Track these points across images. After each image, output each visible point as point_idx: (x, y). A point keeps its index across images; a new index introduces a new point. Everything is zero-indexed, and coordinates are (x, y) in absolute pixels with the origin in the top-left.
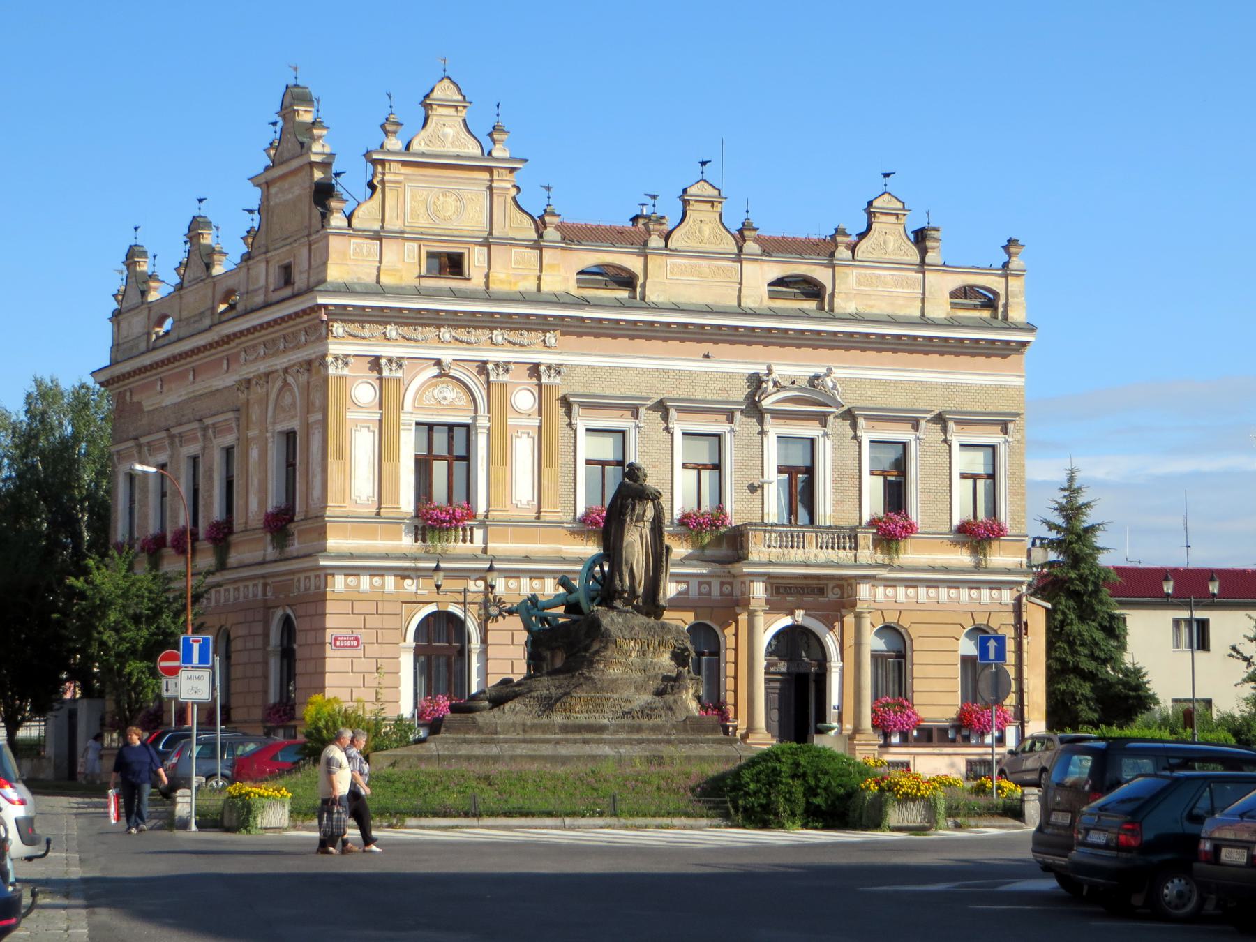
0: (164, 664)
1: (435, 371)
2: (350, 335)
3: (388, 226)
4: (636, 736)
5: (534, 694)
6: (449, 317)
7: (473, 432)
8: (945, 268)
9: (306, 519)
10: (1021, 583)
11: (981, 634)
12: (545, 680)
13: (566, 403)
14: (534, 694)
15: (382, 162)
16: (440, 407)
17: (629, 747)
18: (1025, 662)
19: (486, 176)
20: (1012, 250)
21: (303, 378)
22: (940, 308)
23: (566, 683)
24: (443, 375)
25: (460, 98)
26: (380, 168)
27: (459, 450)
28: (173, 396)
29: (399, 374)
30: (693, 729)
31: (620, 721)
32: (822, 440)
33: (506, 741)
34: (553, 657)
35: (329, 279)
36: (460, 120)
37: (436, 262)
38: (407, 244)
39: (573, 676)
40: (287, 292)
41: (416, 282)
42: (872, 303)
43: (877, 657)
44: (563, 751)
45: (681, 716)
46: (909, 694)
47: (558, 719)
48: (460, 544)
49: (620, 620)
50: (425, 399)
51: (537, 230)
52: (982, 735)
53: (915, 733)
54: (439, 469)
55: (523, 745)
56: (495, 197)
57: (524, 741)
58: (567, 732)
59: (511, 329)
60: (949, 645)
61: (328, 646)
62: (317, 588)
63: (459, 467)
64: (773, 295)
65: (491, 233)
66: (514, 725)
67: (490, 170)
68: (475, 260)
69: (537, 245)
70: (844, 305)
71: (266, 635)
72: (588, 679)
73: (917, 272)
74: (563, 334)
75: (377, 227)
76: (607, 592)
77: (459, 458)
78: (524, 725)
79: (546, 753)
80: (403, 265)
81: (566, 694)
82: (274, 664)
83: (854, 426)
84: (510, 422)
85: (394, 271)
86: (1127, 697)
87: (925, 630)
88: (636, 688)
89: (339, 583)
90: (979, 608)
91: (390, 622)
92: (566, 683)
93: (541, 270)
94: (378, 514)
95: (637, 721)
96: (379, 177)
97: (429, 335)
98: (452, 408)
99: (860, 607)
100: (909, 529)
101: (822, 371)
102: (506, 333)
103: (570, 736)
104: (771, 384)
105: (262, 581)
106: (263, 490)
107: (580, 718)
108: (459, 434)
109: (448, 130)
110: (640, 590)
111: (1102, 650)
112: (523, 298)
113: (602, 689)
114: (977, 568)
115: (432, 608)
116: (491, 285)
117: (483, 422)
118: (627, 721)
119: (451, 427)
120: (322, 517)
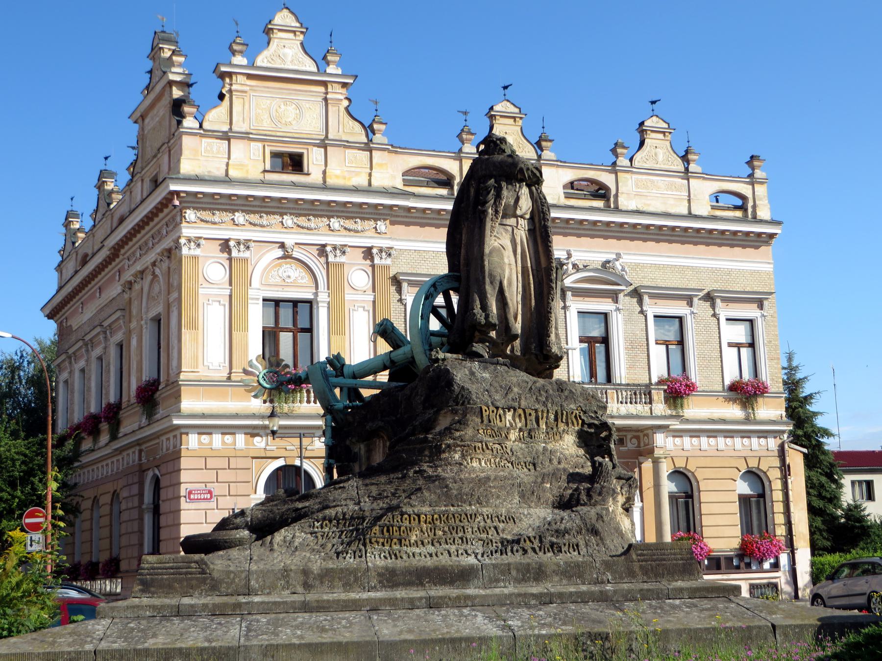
0: (28, 521)
1: (280, 253)
2: (202, 220)
3: (235, 128)
4: (535, 590)
5: (331, 512)
6: (291, 205)
7: (315, 307)
8: (705, 176)
9: (167, 385)
10: (783, 432)
11: (754, 475)
12: (353, 484)
13: (397, 282)
14: (331, 512)
15: (230, 75)
16: (285, 283)
17: (525, 613)
18: (791, 499)
19: (322, 89)
20: (756, 163)
21: (165, 265)
22: (702, 207)
23: (391, 489)
24: (287, 256)
25: (298, 25)
26: (227, 80)
27: (303, 323)
28: (89, 313)
29: (247, 254)
30: (645, 571)
31: (497, 559)
32: (614, 314)
33: (266, 609)
34: (369, 451)
35: (182, 171)
36: (298, 43)
37: (279, 161)
38: (253, 144)
39: (404, 477)
41: (261, 176)
42: (648, 202)
43: (673, 497)
45: (616, 546)
46: (698, 529)
47: (376, 559)
48: (305, 404)
49: (486, 375)
50: (271, 277)
51: (367, 136)
52: (761, 562)
53: (706, 562)
54: (286, 339)
55: (302, 617)
56: (330, 107)
57: (306, 607)
59: (348, 218)
60: (729, 485)
61: (183, 500)
62: (175, 447)
63: (303, 337)
64: (568, 196)
65: (327, 136)
66: (286, 572)
67: (324, 84)
68: (314, 159)
69: (368, 147)
70: (624, 203)
71: (141, 495)
72: (431, 479)
73: (683, 179)
74: (393, 223)
75: (226, 128)
76: (462, 333)
77: (304, 330)
78: (306, 572)
79: (346, 636)
80: (250, 162)
81: (391, 509)
82: (148, 519)
83: (640, 302)
84: (347, 297)
85: (241, 166)
86: (854, 527)
87: (708, 473)
88: (522, 496)
89: (192, 441)
90: (751, 454)
91: (242, 476)
92: (391, 489)
93: (371, 168)
94: (229, 378)
95: (532, 558)
96: (227, 87)
97: (273, 222)
98: (295, 285)
99: (657, 453)
100: (691, 388)
101: (612, 257)
102: (342, 222)
103: (400, 593)
104: (570, 266)
105: (138, 448)
106: (140, 370)
107: (420, 554)
108: (303, 309)
109: (286, 50)
110: (517, 327)
111: (827, 491)
112: (356, 190)
113: (461, 499)
114: (747, 420)
115: (280, 463)
116: (328, 180)
117: (323, 297)
118: (514, 558)
119: (295, 303)
120: (177, 381)
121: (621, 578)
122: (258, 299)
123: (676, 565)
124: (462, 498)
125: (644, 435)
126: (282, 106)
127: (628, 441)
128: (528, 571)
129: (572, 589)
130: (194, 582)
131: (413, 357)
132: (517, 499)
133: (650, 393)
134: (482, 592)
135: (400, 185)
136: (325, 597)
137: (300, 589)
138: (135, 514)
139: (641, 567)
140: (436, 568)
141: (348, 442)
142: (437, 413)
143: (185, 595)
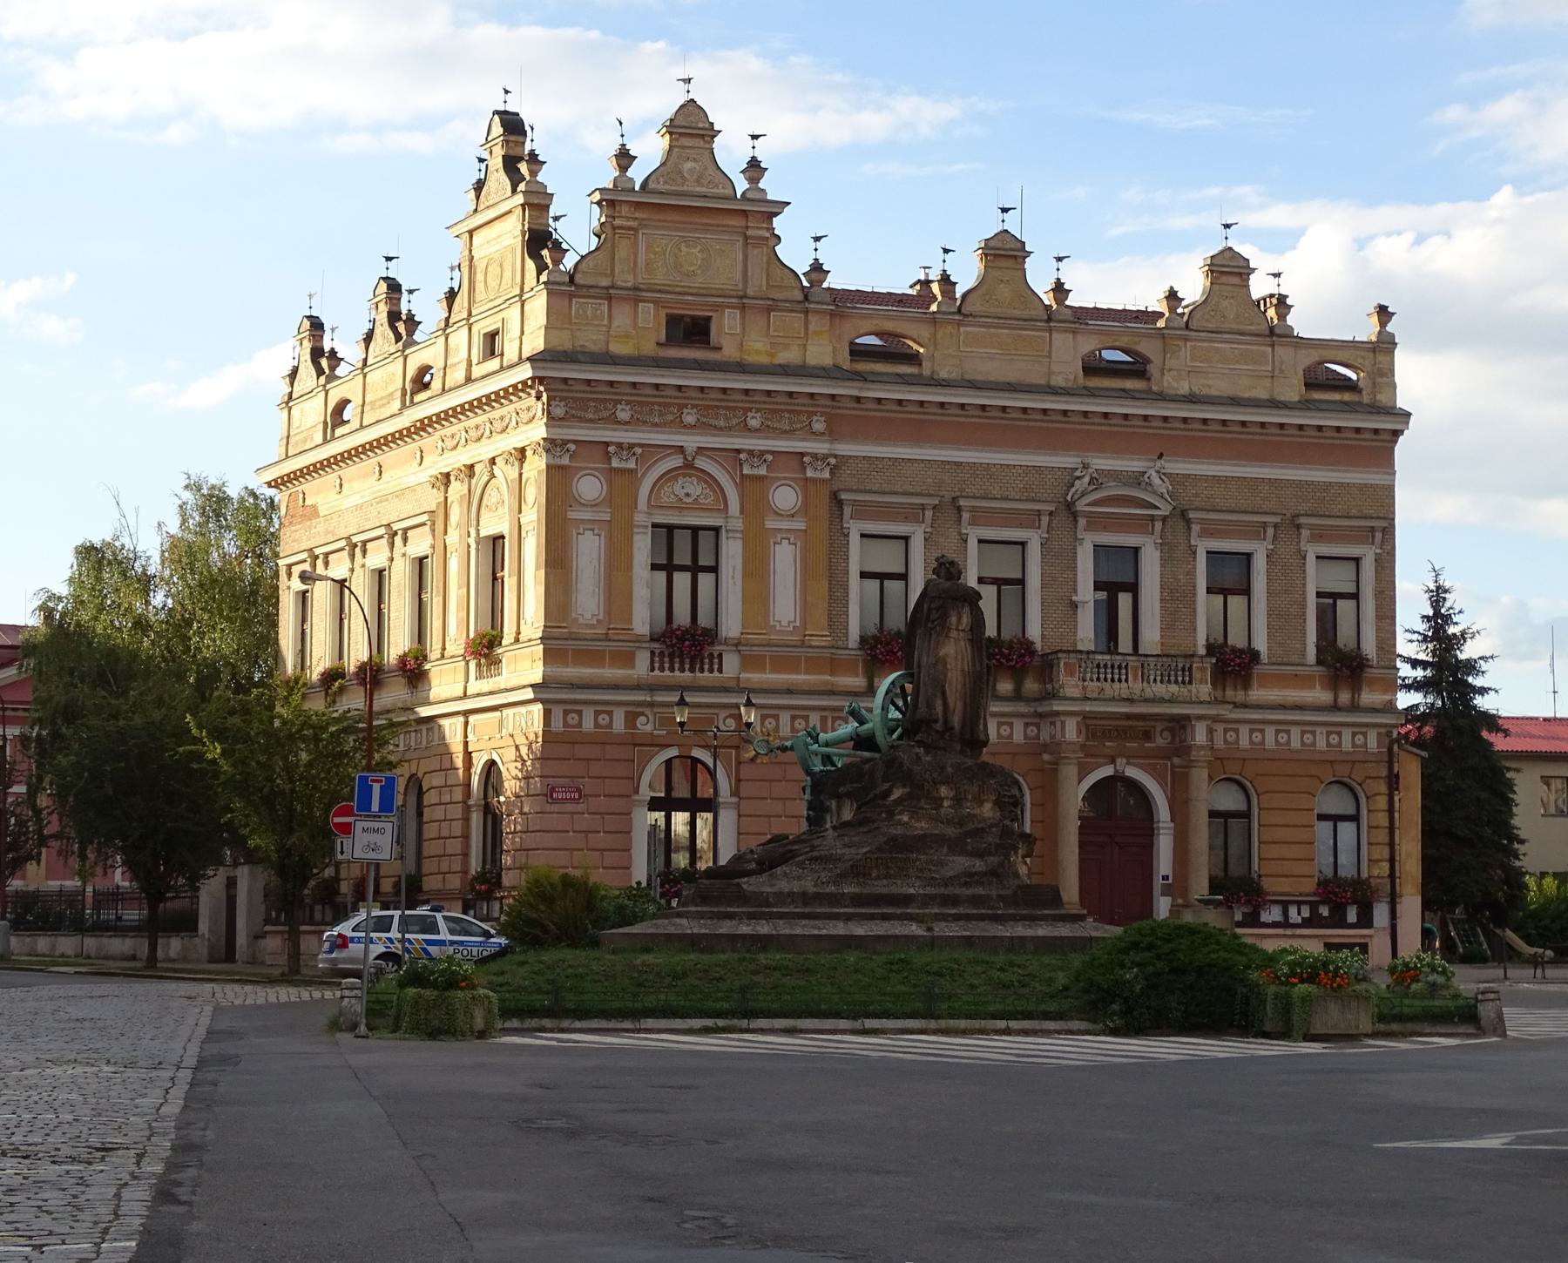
0: (337, 820)
40: (494, 364)
48: (706, 674)
49: (928, 758)
66: (791, 894)
68: (726, 326)
95: (950, 891)
98: (696, 507)
108: (705, 539)
110: (956, 720)
119: (695, 530)
126: (684, 249)
133: (1190, 669)
135: (845, 360)
138: (456, 811)
142: (891, 787)
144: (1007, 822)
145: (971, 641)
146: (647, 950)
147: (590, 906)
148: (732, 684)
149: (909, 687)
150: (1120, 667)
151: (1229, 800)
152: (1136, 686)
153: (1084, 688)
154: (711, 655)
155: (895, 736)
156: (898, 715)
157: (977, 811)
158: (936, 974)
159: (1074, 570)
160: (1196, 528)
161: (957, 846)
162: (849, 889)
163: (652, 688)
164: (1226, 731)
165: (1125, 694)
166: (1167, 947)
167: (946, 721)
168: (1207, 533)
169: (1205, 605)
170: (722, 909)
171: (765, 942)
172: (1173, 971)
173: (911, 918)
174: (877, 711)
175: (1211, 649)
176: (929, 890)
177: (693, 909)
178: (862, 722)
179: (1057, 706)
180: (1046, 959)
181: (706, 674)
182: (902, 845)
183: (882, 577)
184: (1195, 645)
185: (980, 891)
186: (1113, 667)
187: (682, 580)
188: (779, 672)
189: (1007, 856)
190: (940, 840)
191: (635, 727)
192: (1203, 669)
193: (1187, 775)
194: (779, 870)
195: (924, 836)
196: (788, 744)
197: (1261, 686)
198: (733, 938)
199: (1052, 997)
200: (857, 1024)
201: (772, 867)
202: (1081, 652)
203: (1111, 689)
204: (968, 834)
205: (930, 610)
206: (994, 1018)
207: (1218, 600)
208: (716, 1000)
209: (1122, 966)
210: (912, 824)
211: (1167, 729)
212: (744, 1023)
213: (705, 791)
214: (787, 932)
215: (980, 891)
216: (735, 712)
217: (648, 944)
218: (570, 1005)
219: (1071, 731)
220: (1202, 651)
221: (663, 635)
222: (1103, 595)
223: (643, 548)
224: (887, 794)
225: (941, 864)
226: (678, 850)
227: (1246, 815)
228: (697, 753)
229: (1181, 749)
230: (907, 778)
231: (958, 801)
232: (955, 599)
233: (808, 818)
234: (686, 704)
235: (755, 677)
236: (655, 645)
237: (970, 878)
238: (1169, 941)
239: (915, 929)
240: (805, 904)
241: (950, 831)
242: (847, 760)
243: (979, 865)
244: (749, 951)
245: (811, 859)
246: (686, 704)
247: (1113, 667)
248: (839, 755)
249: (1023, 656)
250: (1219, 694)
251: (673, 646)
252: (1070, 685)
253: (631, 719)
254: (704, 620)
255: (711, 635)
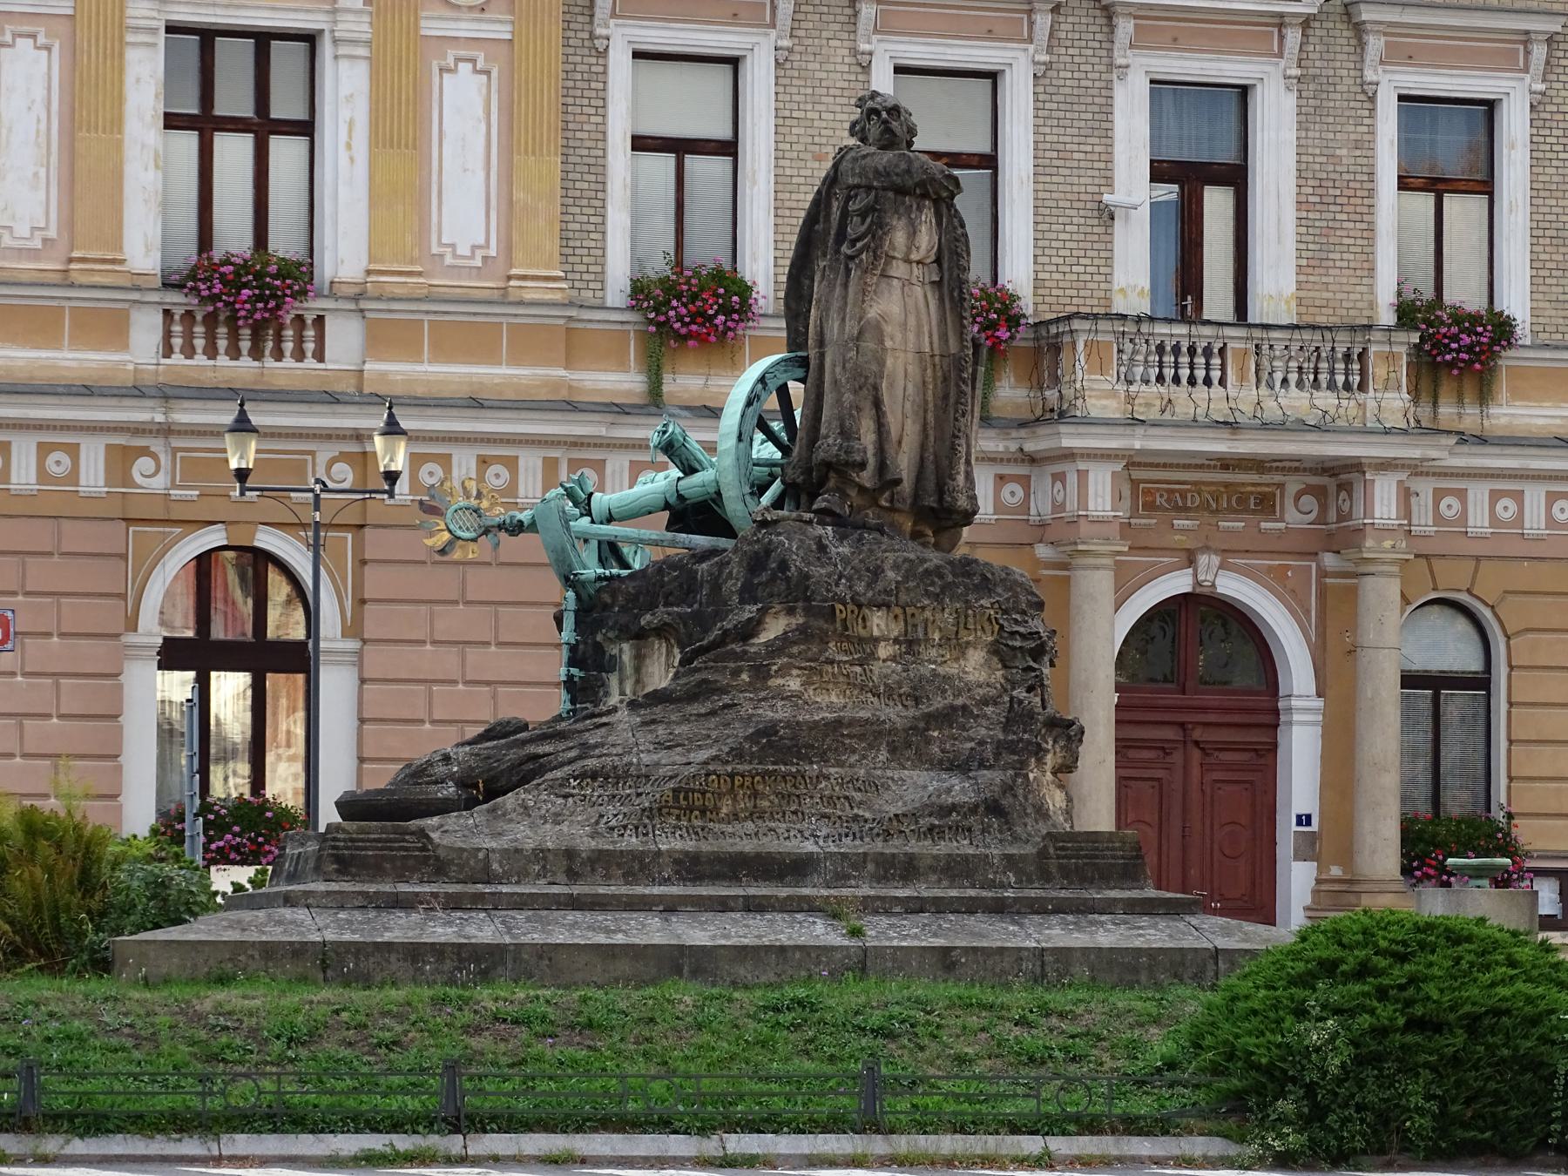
30: (1066, 873)
34: (639, 658)
44: (698, 933)
49: (845, 550)
55: (571, 916)
57: (575, 904)
58: (697, 878)
66: (540, 854)
88: (893, 750)
95: (895, 847)
108: (286, 61)
110: (904, 463)
119: (263, 40)
121: (1030, 881)
122: (153, 31)
123: (1113, 865)
124: (799, 752)
125: (1340, 487)
127: (1289, 502)
128: (893, 866)
129: (954, 893)
130: (411, 862)
131: (719, 493)
132: (883, 755)
134: (825, 892)
136: (601, 890)
137: (562, 878)
139: (1061, 867)
140: (758, 855)
141: (599, 638)
142: (763, 612)
143: (402, 878)
144: (1020, 693)
145: (938, 285)
146: (223, 980)
147: (87, 882)
148: (346, 386)
149: (796, 389)
150: (1208, 352)
151: (1451, 649)
152: (1243, 396)
153: (1130, 399)
154: (300, 319)
155: (766, 499)
156: (770, 451)
157: (952, 669)
158: (877, 1032)
159: (1107, 135)
160: (1375, 44)
161: (907, 745)
162: (672, 843)
163: (167, 394)
164: (1439, 494)
165: (1220, 411)
166: (1399, 973)
167: (882, 467)
168: (1398, 55)
169: (1395, 214)
170: (387, 888)
171: (484, 962)
172: (1415, 1024)
173: (810, 907)
174: (728, 443)
175: (1406, 314)
176: (848, 846)
177: (321, 887)
178: (689, 470)
179: (1070, 439)
180: (1121, 1000)
181: (289, 362)
182: (783, 751)
183: (680, 147)
184: (1372, 305)
185: (964, 847)
186: (1192, 351)
187: (233, 151)
188: (450, 360)
189: (1023, 764)
190: (872, 733)
191: (128, 481)
192: (1390, 358)
193: (1352, 594)
194: (509, 800)
195: (838, 723)
196: (525, 516)
197: (1517, 394)
198: (414, 953)
199: (1140, 1083)
200: (710, 1146)
201: (492, 793)
202: (1124, 317)
203: (1187, 402)
204: (934, 719)
205: (845, 214)
206: (1015, 1130)
207: (1424, 203)
208: (389, 1092)
209: (1301, 1013)
210: (807, 696)
211: (1309, 490)
212: (454, 1144)
213: (285, 624)
214: (537, 938)
215: (964, 847)
216: (353, 448)
217: (226, 963)
218: (61, 1104)
219: (1101, 494)
220: (1387, 317)
221: (193, 275)
222: (1169, 192)
223: (146, 81)
224: (749, 631)
225: (874, 786)
226: (227, 756)
227: (1481, 682)
228: (267, 540)
229: (1341, 536)
230: (798, 594)
231: (910, 644)
232: (901, 191)
233: (569, 683)
234: (254, 430)
235: (395, 371)
236: (174, 298)
237: (942, 818)
238: (1402, 958)
239: (820, 932)
240: (573, 875)
241: (894, 714)
242: (657, 554)
243: (959, 790)
244: (451, 982)
245: (582, 776)
246: (254, 430)
247: (1192, 351)
248: (638, 542)
249: (991, 326)
250: (1425, 411)
251: (214, 298)
252: (1098, 390)
253: (120, 461)
254: (284, 242)
255: (298, 276)
